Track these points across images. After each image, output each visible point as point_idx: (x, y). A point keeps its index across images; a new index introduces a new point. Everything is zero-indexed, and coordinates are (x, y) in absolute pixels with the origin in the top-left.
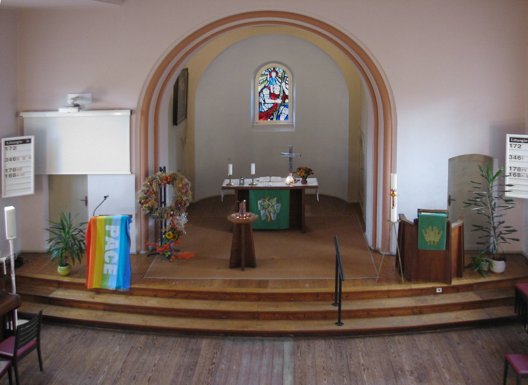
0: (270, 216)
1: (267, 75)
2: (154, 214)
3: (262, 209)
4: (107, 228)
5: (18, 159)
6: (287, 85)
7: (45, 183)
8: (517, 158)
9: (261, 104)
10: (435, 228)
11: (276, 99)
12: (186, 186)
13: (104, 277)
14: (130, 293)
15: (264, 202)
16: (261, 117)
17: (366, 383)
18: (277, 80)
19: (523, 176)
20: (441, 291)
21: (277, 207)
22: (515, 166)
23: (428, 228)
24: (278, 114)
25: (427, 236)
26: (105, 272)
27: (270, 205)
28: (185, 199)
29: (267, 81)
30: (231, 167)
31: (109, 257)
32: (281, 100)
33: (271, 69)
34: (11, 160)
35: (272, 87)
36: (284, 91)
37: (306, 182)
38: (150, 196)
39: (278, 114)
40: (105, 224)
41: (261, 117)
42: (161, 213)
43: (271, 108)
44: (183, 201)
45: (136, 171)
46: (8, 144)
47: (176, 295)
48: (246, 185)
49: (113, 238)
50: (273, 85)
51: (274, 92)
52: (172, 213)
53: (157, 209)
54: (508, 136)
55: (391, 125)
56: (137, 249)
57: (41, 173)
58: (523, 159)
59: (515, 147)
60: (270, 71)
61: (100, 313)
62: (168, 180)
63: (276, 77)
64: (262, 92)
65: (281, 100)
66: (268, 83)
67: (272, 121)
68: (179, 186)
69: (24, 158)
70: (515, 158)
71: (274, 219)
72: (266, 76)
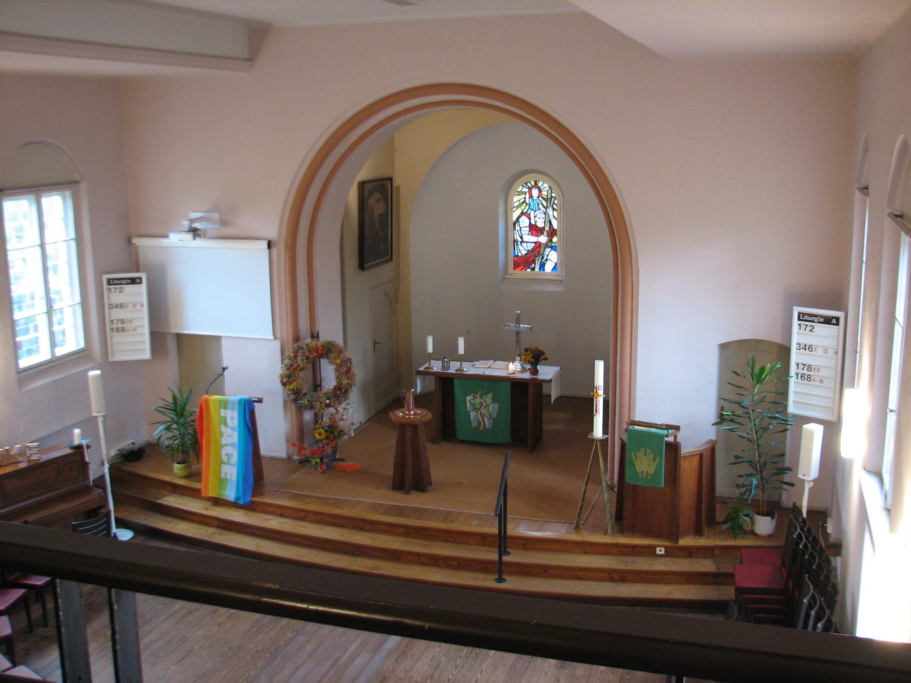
0: (483, 421)
1: (526, 193)
2: (300, 401)
4: (223, 412)
6: (555, 211)
7: (172, 345)
8: (807, 348)
9: (517, 243)
10: (648, 451)
11: (539, 236)
12: (347, 363)
13: (222, 482)
14: (250, 507)
15: (474, 399)
16: (516, 265)
17: (488, 658)
18: (540, 203)
20: (663, 552)
21: (493, 408)
22: (804, 363)
24: (543, 261)
25: (639, 463)
26: (223, 476)
27: (483, 405)
28: (346, 383)
29: (525, 204)
30: (461, 342)
31: (227, 454)
32: (547, 238)
33: (530, 183)
36: (550, 222)
37: (535, 371)
38: (294, 374)
39: (543, 261)
41: (516, 265)
42: (312, 401)
45: (281, 335)
46: (111, 283)
48: (452, 370)
49: (230, 428)
50: (535, 211)
51: (536, 222)
52: (328, 401)
53: (306, 394)
54: (796, 310)
55: (630, 284)
56: (288, 452)
57: (164, 331)
58: (815, 351)
60: (530, 186)
61: (212, 530)
62: (320, 352)
63: (538, 197)
65: (547, 238)
66: (528, 207)
70: (804, 348)
71: (489, 427)
72: (524, 196)
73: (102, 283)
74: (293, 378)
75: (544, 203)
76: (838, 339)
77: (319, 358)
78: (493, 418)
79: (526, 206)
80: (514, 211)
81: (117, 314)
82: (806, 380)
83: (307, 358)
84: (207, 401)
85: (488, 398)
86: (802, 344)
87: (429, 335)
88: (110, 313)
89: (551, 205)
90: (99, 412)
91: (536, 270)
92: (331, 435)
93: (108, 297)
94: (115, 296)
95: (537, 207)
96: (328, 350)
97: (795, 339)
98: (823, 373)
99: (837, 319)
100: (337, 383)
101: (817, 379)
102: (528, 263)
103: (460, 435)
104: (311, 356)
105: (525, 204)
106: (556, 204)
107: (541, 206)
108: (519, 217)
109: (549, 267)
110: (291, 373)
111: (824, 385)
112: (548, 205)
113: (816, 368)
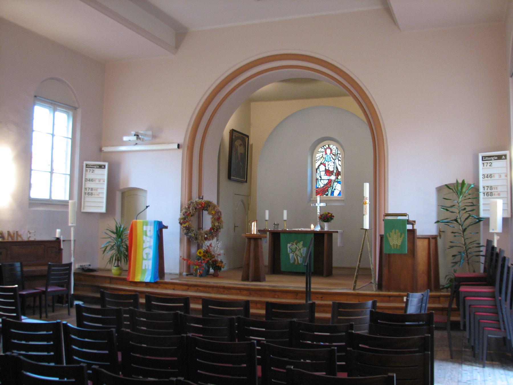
0: (297, 258)
1: (323, 152)
2: (190, 234)
3: (291, 252)
4: (145, 228)
5: (95, 180)
6: (339, 161)
8: (489, 176)
10: (397, 231)
11: (331, 176)
15: (292, 246)
18: (331, 157)
19: (494, 195)
21: (303, 251)
23: (391, 232)
24: (333, 190)
27: (297, 249)
29: (323, 158)
31: (146, 254)
34: (89, 180)
35: (327, 163)
36: (337, 168)
38: (187, 217)
39: (333, 190)
40: (143, 225)
43: (327, 184)
44: (215, 227)
47: (188, 289)
49: (149, 237)
50: (328, 162)
51: (329, 168)
56: (180, 270)
58: (494, 177)
59: (487, 166)
60: (326, 148)
63: (330, 154)
64: (319, 168)
65: (335, 177)
66: (324, 160)
67: (327, 196)
68: (212, 212)
69: (100, 181)
70: (487, 177)
72: (322, 154)
73: (83, 166)
74: (186, 219)
75: (334, 157)
76: (507, 167)
77: (203, 210)
78: (303, 257)
79: (323, 159)
80: (316, 162)
81: (89, 185)
82: (490, 195)
83: (196, 209)
84: (136, 223)
85: (300, 245)
86: (486, 174)
87: (267, 210)
88: (85, 184)
89: (337, 158)
90: (72, 224)
91: (329, 195)
92: (207, 254)
93: (85, 184)
94: (89, 175)
95: (329, 159)
96: (207, 206)
97: (481, 172)
98: (500, 189)
99: (505, 156)
100: (212, 225)
101: (496, 193)
102: (324, 192)
103: (283, 269)
104: (198, 207)
105: (323, 158)
106: (340, 157)
107: (332, 159)
108: (319, 165)
109: (336, 193)
110: (185, 217)
111: (501, 196)
112: (336, 158)
113: (495, 187)
